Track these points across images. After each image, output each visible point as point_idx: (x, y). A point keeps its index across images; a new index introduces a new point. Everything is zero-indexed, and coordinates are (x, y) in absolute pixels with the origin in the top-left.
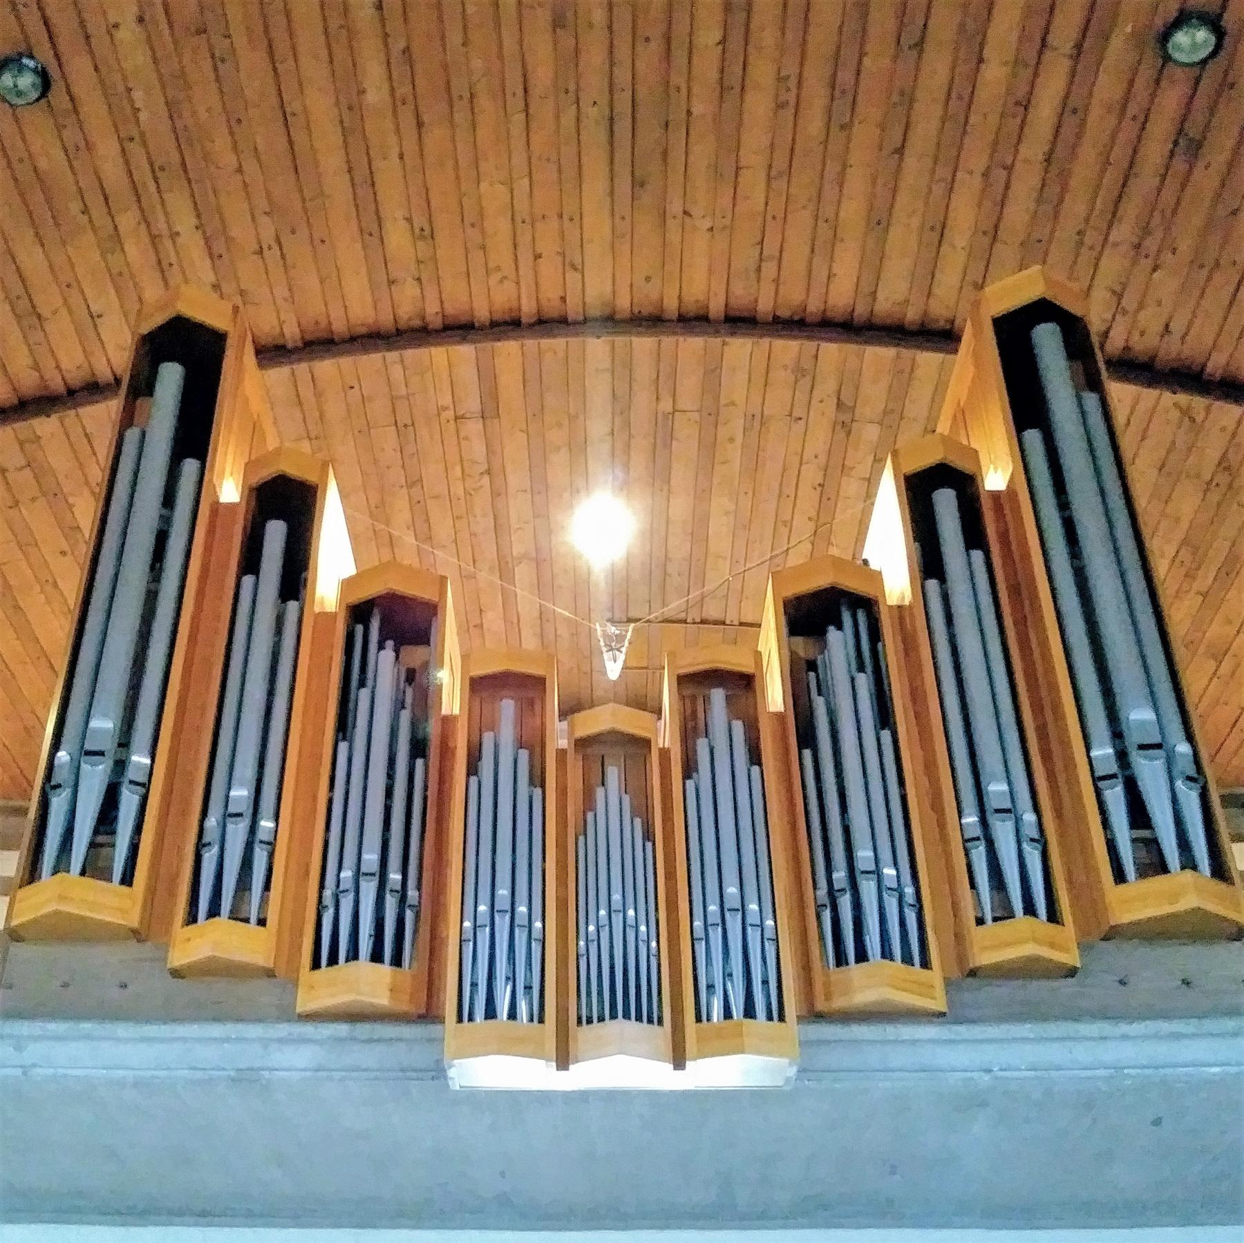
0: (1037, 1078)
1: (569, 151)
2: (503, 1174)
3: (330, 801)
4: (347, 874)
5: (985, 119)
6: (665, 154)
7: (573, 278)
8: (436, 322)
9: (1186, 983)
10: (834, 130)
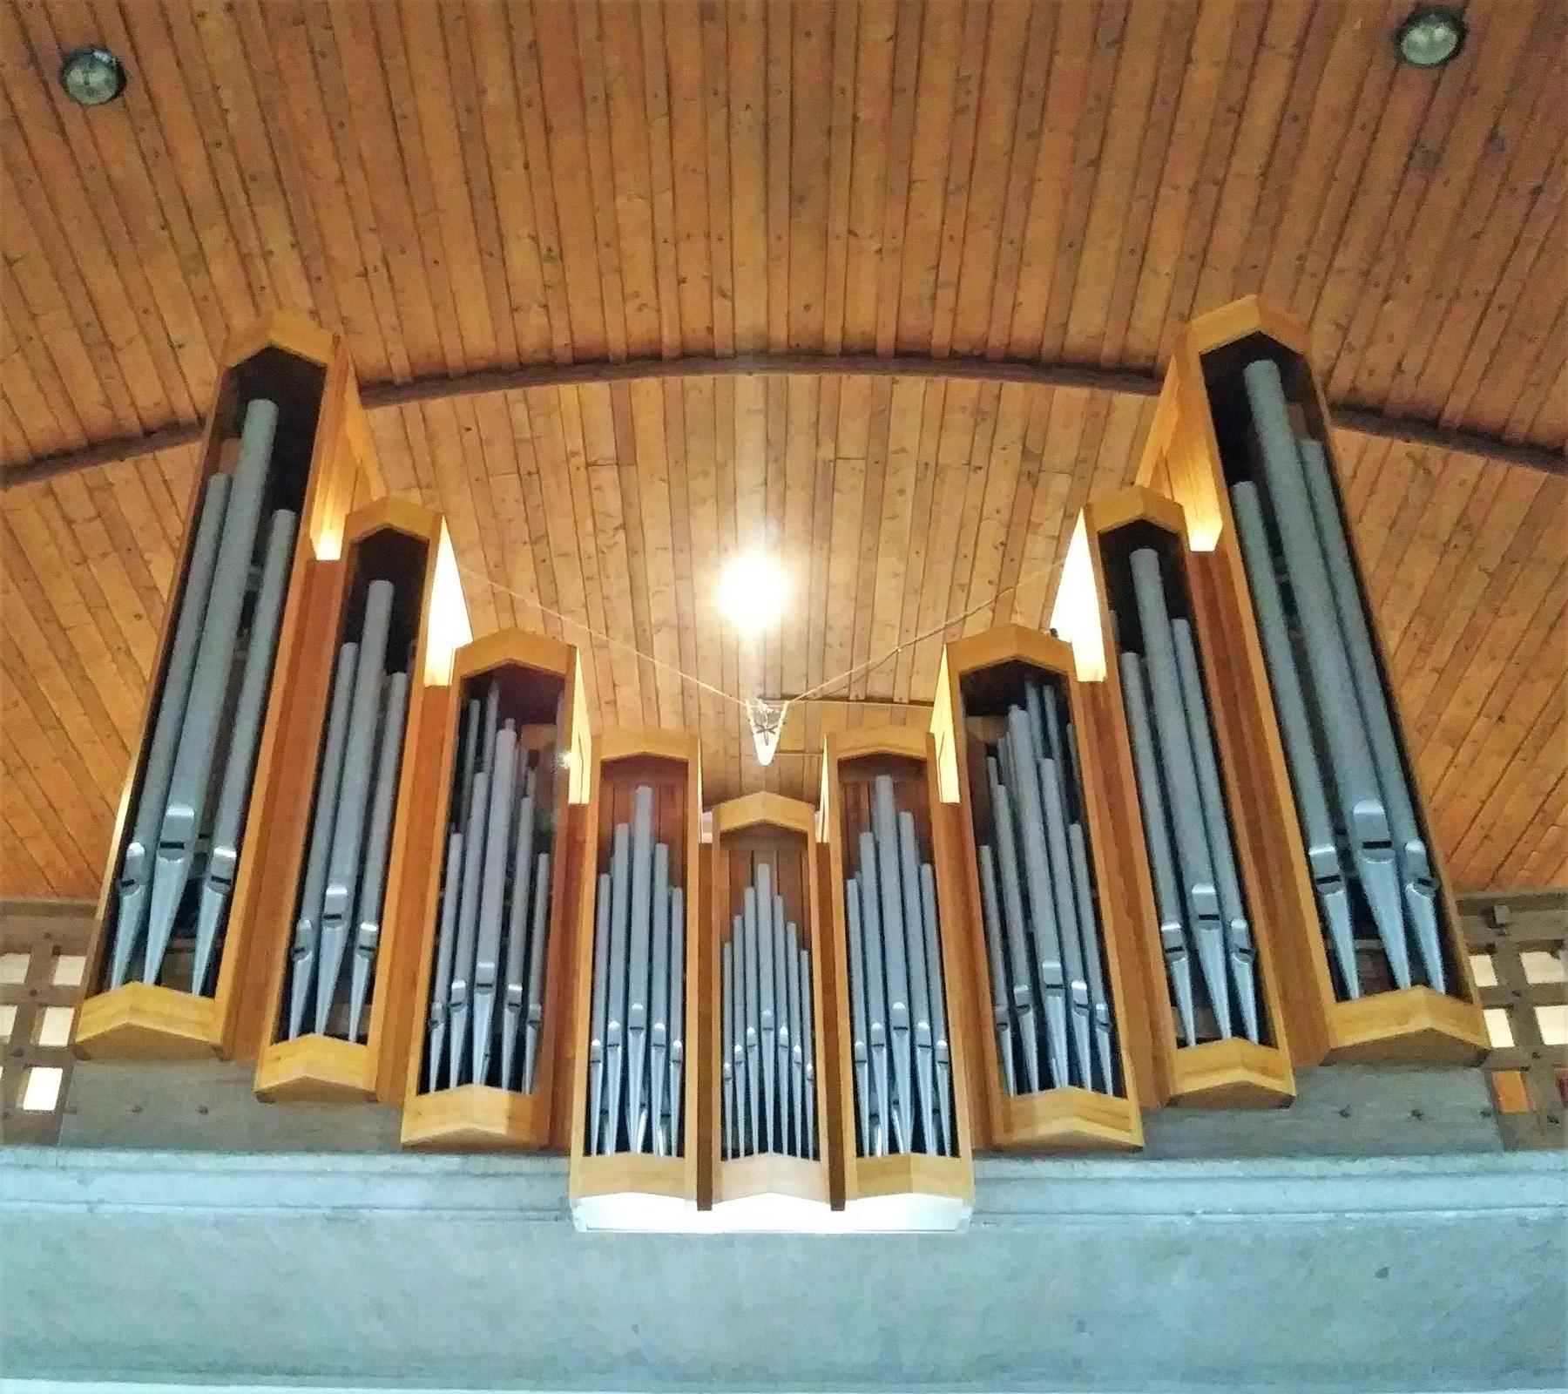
3: (441, 902)
4: (459, 985)
7: (721, 305)
8: (565, 355)
9: (1417, 1114)
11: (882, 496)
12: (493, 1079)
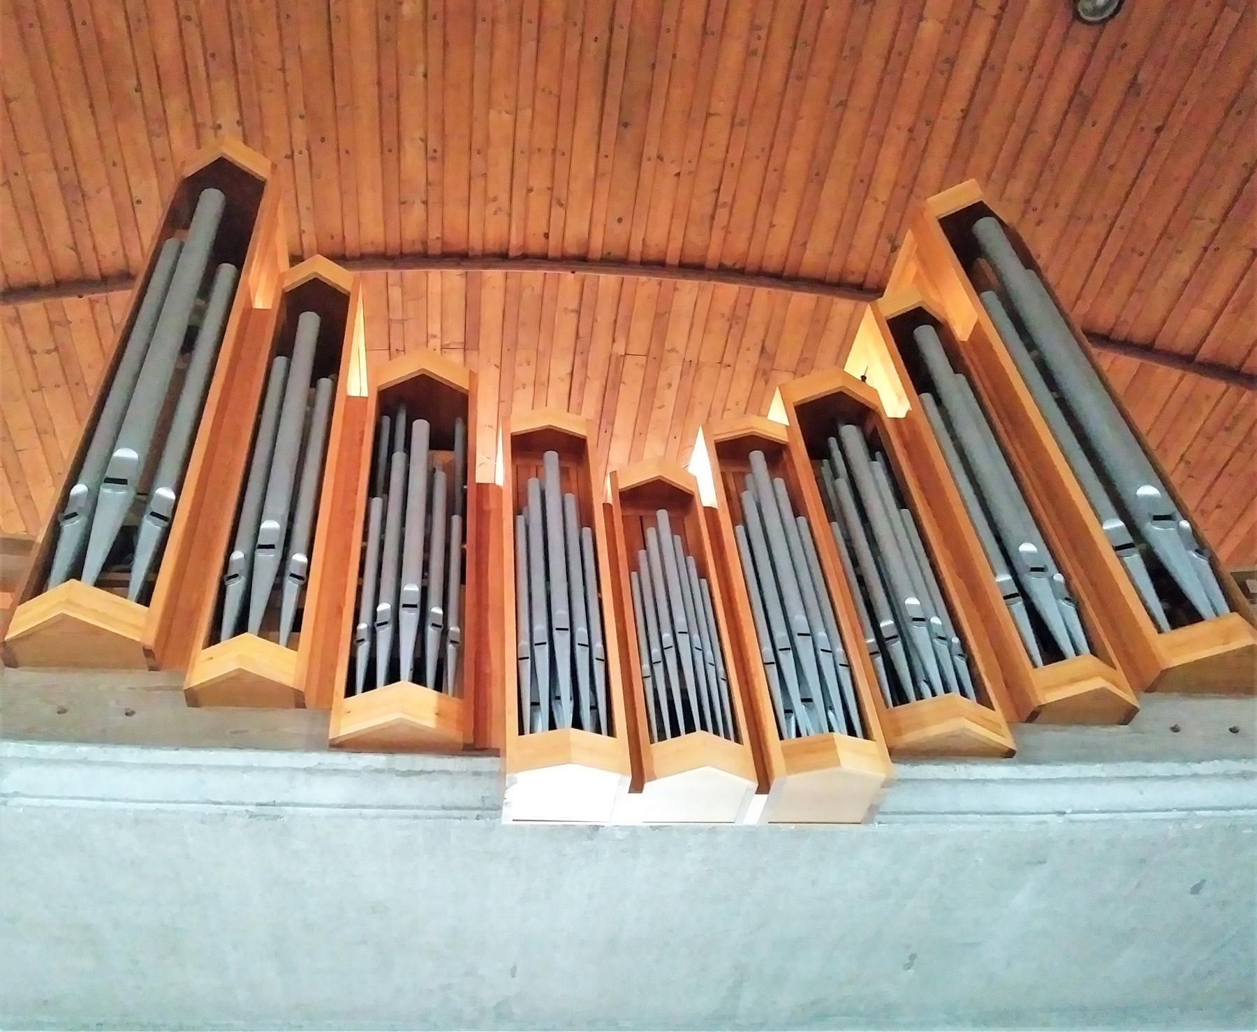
0: (1111, 820)
1: (569, 85)
2: (513, 972)
3: (364, 551)
4: (384, 607)
5: (914, 84)
6: (649, 95)
7: (557, 212)
8: (435, 248)
9: (1234, 730)
10: (792, 81)
11: (655, 388)
12: (418, 677)
